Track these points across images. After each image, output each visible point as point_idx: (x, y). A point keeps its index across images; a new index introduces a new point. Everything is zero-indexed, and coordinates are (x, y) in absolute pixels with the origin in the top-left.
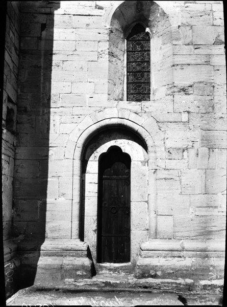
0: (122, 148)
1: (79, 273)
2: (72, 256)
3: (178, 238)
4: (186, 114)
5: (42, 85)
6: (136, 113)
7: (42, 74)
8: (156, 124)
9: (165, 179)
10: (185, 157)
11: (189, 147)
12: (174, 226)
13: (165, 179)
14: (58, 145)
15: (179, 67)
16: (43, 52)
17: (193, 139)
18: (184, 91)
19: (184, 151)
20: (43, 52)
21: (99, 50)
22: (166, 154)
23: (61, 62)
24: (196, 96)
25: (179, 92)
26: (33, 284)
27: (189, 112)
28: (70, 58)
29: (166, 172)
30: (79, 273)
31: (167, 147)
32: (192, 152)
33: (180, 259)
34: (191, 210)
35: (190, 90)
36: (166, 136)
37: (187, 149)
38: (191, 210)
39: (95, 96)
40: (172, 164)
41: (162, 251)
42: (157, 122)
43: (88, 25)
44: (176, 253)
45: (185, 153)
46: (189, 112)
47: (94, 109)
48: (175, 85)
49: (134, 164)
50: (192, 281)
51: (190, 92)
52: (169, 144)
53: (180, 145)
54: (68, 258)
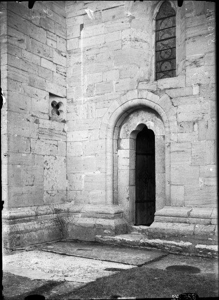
0: (147, 125)
1: (105, 231)
2: (103, 218)
3: (188, 206)
4: (197, 87)
5: (82, 78)
6: (152, 92)
7: (82, 69)
8: (169, 100)
9: (177, 151)
10: (196, 129)
11: (200, 119)
12: (185, 194)
13: (177, 151)
14: (95, 128)
15: (191, 40)
16: (82, 49)
17: (203, 111)
18: (195, 64)
19: (194, 124)
20: (82, 49)
21: (123, 38)
22: (177, 128)
23: (95, 55)
24: (207, 67)
25: (191, 65)
26: (149, 225)
27: (199, 85)
28: (101, 50)
29: (178, 145)
30: (105, 231)
31: (179, 121)
32: (202, 124)
33: (185, 224)
34: (201, 180)
35: (202, 62)
36: (178, 111)
37: (197, 121)
38: (201, 180)
39: (121, 81)
40: (184, 137)
41: (171, 216)
42: (171, 98)
43: (114, 17)
44: (182, 219)
45: (196, 125)
46: (199, 85)
47: (120, 93)
48: (187, 59)
49: (157, 139)
50: (190, 244)
51: (201, 64)
52: (181, 118)
53: (191, 118)
54: (100, 220)
